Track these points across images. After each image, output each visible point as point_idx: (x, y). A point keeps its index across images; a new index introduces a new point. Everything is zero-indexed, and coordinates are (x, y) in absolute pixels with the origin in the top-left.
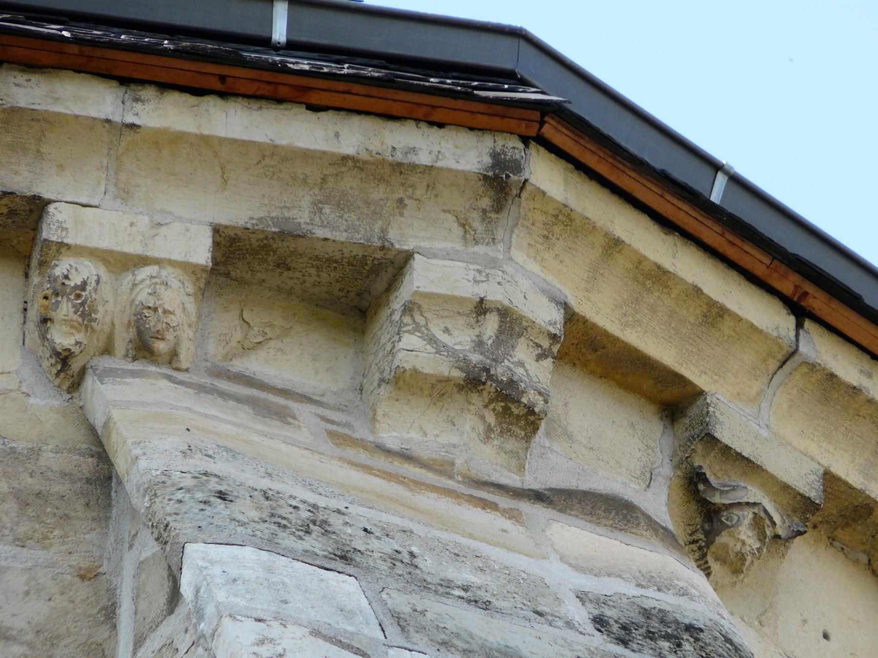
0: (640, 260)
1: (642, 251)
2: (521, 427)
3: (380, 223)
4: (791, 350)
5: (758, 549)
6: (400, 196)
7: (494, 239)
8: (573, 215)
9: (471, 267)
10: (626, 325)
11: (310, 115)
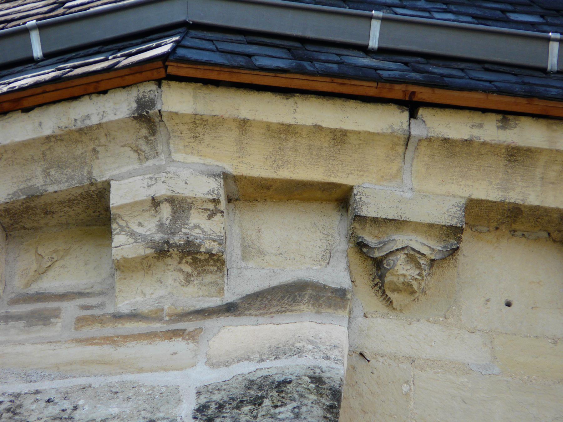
0: (268, 126)
1: (265, 119)
2: (211, 265)
3: (86, 168)
4: (407, 136)
5: (418, 275)
6: (92, 147)
7: (157, 153)
8: (205, 118)
9: (146, 177)
10: (278, 167)
11: (25, 116)
